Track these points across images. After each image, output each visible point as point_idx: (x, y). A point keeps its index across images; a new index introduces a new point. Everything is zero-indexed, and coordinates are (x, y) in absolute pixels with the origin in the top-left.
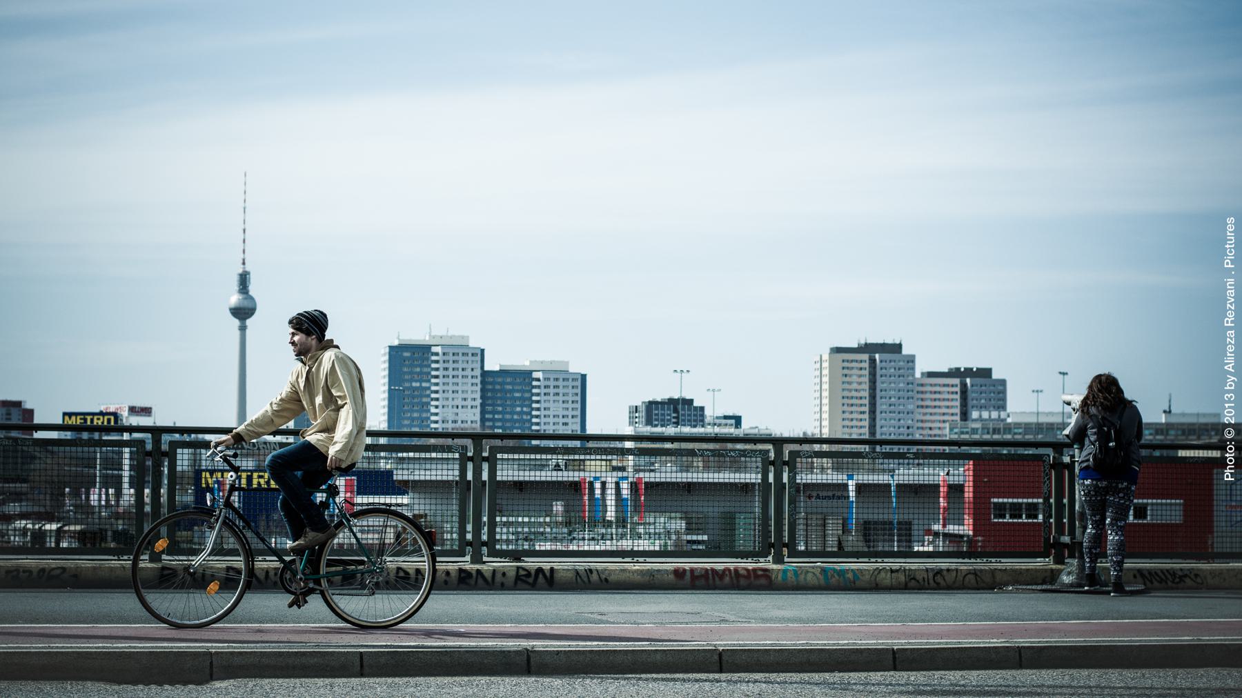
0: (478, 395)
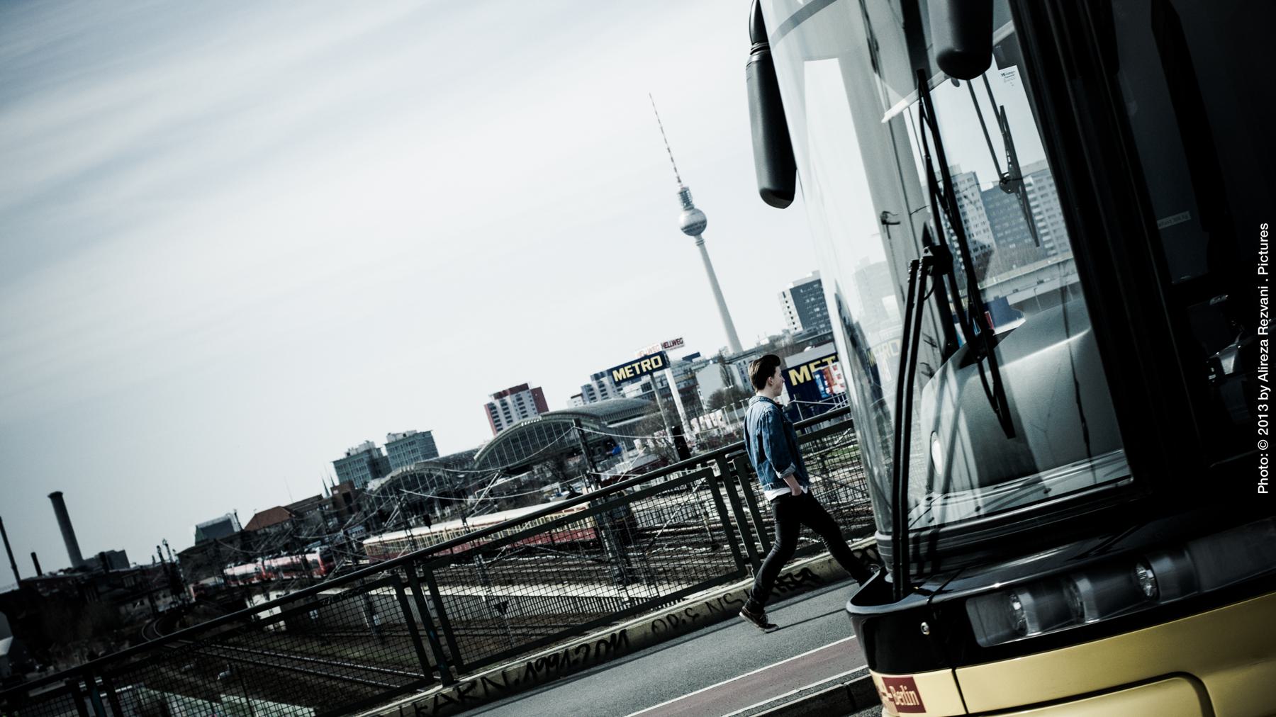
0: (985, 218)
